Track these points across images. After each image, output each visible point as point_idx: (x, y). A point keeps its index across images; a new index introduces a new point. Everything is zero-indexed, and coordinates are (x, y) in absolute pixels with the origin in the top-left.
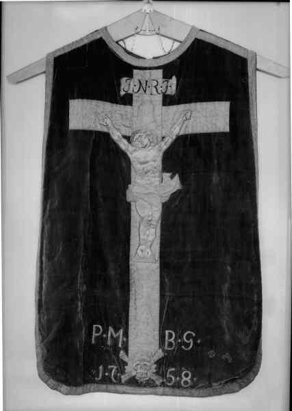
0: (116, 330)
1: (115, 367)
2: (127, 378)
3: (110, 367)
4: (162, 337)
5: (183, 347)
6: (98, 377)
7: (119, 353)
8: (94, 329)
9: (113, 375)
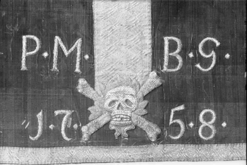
0: (69, 44)
1: (68, 113)
2: (92, 130)
3: (57, 113)
4: (157, 48)
5: (198, 66)
6: (35, 133)
7: (77, 83)
8: (166, 43)
9: (63, 128)
